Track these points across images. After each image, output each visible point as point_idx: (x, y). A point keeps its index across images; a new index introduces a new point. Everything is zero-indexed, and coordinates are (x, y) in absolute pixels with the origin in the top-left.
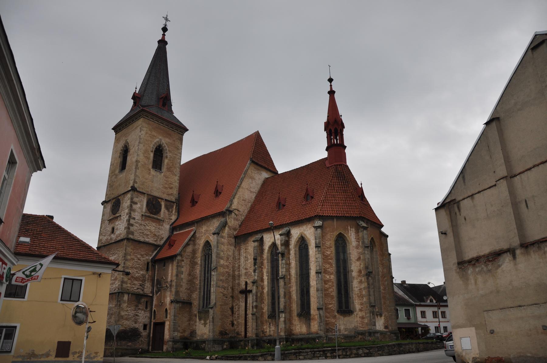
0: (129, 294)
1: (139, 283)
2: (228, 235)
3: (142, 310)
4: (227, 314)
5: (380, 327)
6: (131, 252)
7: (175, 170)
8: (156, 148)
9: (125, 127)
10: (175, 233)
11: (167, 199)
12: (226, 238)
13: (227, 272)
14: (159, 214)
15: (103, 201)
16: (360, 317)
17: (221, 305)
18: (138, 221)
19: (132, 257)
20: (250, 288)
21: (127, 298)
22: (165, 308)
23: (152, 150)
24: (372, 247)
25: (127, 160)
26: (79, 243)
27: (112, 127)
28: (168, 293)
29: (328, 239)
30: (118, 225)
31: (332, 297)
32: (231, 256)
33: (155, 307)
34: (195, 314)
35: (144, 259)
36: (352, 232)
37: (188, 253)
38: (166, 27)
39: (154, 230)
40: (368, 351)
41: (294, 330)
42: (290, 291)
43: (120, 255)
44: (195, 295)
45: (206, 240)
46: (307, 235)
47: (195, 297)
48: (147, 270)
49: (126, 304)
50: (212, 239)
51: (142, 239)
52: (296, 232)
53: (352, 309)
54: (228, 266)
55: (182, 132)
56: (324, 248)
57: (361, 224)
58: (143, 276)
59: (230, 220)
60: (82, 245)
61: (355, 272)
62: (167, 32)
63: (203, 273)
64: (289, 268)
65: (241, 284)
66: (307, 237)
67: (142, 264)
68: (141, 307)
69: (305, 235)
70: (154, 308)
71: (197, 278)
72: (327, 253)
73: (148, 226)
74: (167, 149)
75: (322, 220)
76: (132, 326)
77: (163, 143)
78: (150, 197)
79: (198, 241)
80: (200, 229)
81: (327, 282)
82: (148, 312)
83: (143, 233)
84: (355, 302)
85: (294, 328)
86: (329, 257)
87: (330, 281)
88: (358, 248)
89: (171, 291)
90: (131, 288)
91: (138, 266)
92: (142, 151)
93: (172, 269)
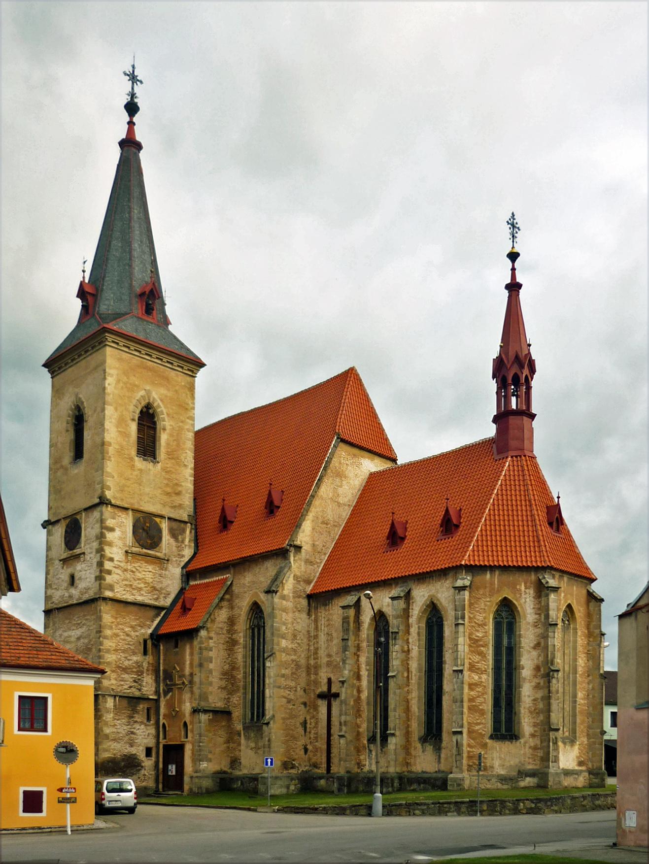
0: (115, 696)
1: (132, 678)
2: (294, 592)
3: (142, 723)
4: (294, 733)
5: (568, 764)
6: (112, 623)
7: (184, 455)
8: (141, 412)
9: (72, 364)
10: (192, 583)
11: (172, 516)
12: (291, 599)
13: (293, 661)
14: (158, 548)
15: (45, 521)
16: (530, 747)
17: (284, 719)
18: (119, 563)
19: (115, 631)
20: (336, 688)
21: (112, 704)
22: (183, 722)
23: (133, 416)
24: (568, 620)
25: (85, 438)
26: (31, 635)
27: (43, 362)
28: (187, 696)
29: (481, 609)
30: (81, 571)
31: (482, 713)
32: (300, 632)
33: (164, 719)
34: (237, 731)
35: (137, 634)
36: (527, 596)
37: (219, 623)
38: (136, 100)
39: (152, 578)
40: (533, 806)
41: (412, 763)
42: (408, 699)
43: (91, 628)
44: (236, 699)
45: (254, 600)
46: (441, 600)
47: (236, 702)
48: (145, 653)
49: (112, 715)
50: (264, 600)
51: (130, 598)
52: (422, 594)
53: (516, 733)
54: (295, 651)
55: (192, 371)
56: (473, 626)
57: (547, 582)
58: (139, 665)
59: (297, 564)
60: (38, 638)
61: (527, 670)
62: (138, 113)
63: (249, 661)
64: (408, 659)
65: (321, 682)
66: (441, 604)
67: (134, 644)
68: (138, 718)
69: (438, 600)
70: (162, 721)
71: (238, 668)
72: (478, 635)
73: (140, 572)
74: (165, 411)
75: (471, 574)
76: (126, 751)
77: (154, 399)
78: (139, 515)
79: (237, 601)
80: (239, 579)
81: (474, 687)
82: (151, 727)
83: (131, 585)
84: (523, 721)
85: (412, 761)
86: (481, 643)
87: (479, 685)
88: (536, 626)
89: (192, 692)
90: (118, 686)
91: (126, 647)
92: (113, 421)
93: (192, 654)
